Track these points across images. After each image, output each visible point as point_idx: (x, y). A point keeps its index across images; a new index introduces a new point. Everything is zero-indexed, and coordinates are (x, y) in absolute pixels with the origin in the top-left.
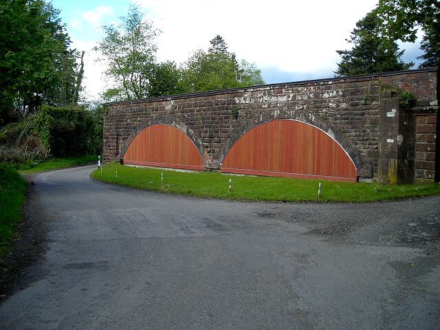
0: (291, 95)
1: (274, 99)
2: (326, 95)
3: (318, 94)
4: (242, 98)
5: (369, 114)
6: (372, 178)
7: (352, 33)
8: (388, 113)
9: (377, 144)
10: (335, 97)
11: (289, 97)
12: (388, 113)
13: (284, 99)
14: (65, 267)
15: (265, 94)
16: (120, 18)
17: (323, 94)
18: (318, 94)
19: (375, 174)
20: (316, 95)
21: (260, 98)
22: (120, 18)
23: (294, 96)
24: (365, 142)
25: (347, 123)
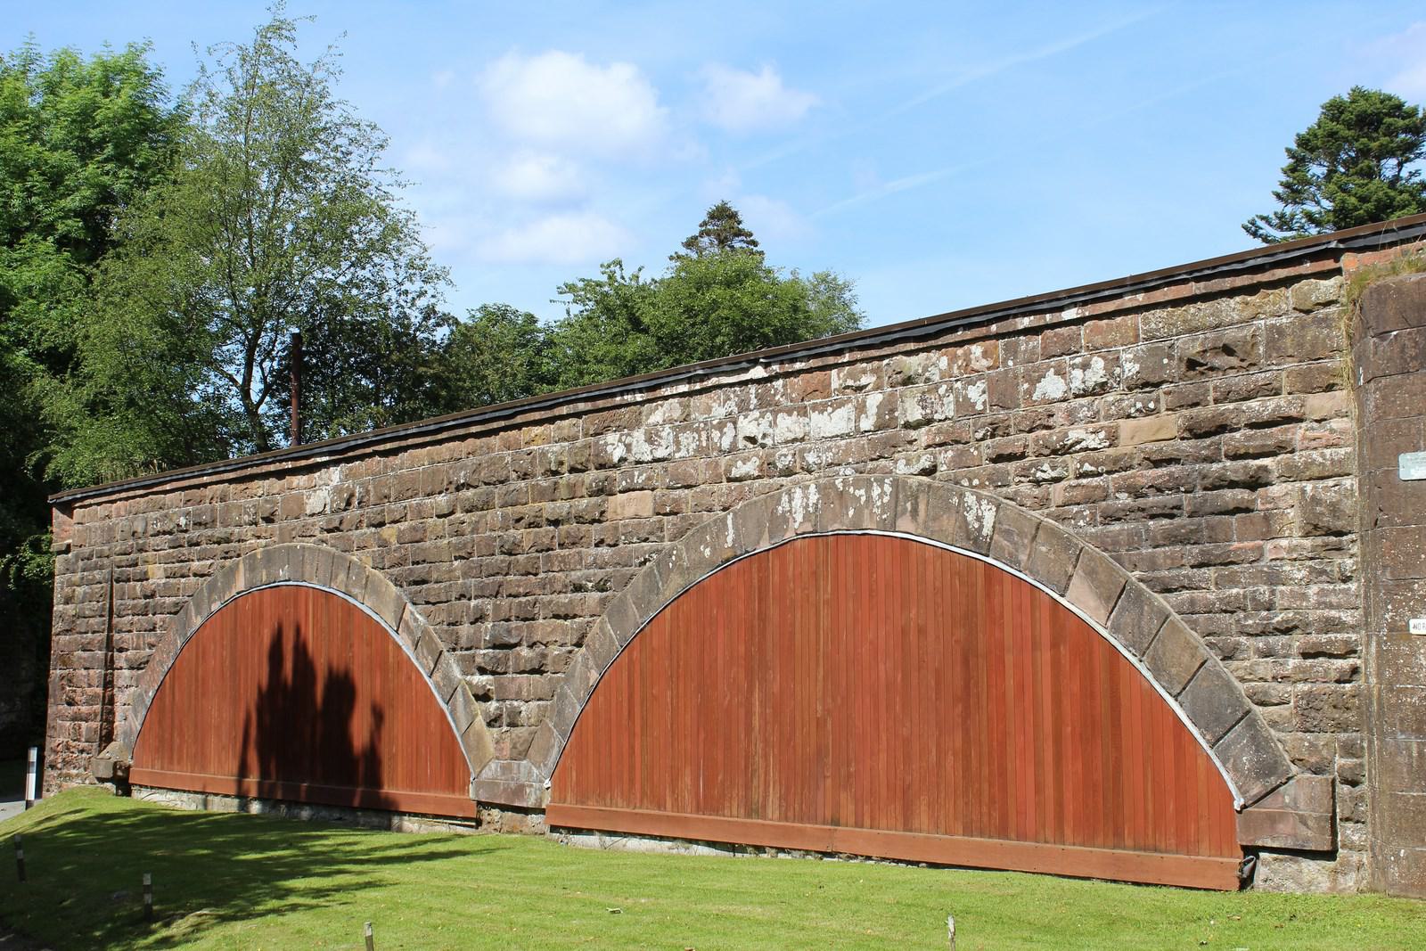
0: (874, 400)
1: (788, 425)
2: (1052, 386)
3: (1010, 381)
4: (639, 435)
5: (1291, 474)
6: (1330, 855)
7: (1275, 213)
8: (1404, 459)
9: (1350, 652)
10: (1102, 389)
11: (861, 409)
12: (1404, 459)
13: (833, 422)
14: (1296, 627)
15: (744, 408)
16: (671, 258)
17: (1034, 382)
18: (1010, 381)
19: (1348, 832)
20: (1002, 395)
21: (721, 427)
22: (671, 258)
23: (888, 408)
24: (1279, 641)
25: (1173, 539)
